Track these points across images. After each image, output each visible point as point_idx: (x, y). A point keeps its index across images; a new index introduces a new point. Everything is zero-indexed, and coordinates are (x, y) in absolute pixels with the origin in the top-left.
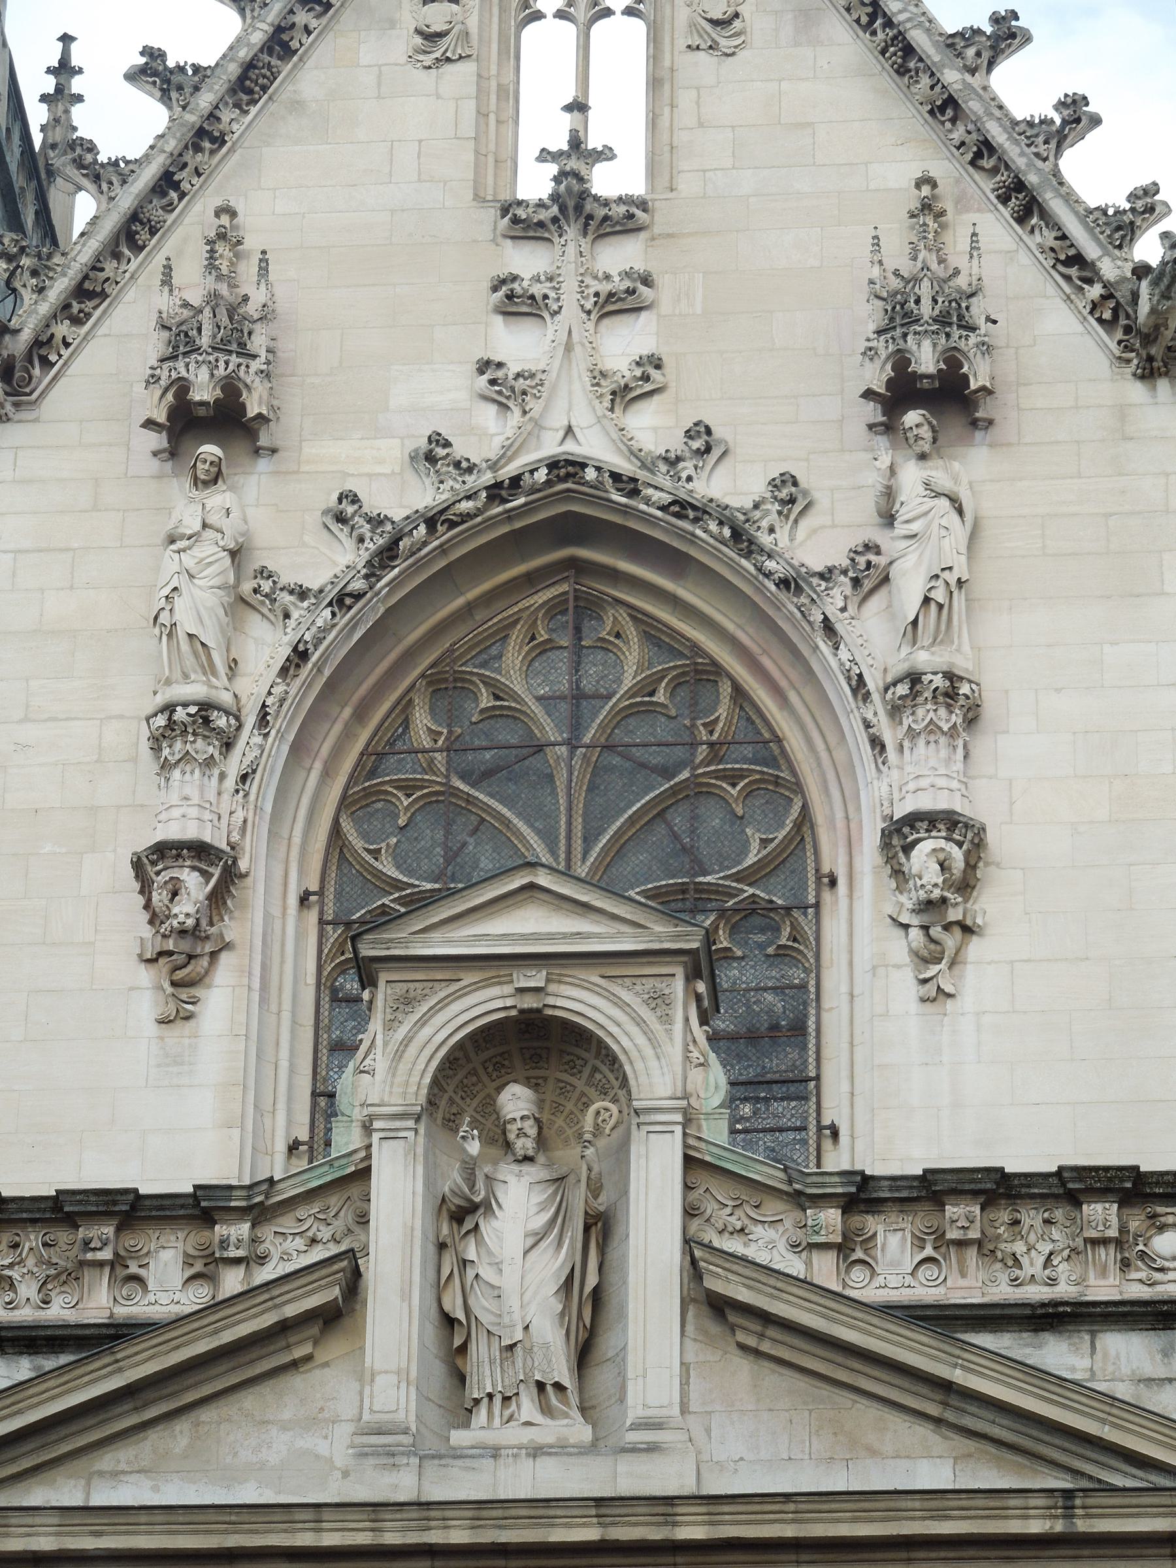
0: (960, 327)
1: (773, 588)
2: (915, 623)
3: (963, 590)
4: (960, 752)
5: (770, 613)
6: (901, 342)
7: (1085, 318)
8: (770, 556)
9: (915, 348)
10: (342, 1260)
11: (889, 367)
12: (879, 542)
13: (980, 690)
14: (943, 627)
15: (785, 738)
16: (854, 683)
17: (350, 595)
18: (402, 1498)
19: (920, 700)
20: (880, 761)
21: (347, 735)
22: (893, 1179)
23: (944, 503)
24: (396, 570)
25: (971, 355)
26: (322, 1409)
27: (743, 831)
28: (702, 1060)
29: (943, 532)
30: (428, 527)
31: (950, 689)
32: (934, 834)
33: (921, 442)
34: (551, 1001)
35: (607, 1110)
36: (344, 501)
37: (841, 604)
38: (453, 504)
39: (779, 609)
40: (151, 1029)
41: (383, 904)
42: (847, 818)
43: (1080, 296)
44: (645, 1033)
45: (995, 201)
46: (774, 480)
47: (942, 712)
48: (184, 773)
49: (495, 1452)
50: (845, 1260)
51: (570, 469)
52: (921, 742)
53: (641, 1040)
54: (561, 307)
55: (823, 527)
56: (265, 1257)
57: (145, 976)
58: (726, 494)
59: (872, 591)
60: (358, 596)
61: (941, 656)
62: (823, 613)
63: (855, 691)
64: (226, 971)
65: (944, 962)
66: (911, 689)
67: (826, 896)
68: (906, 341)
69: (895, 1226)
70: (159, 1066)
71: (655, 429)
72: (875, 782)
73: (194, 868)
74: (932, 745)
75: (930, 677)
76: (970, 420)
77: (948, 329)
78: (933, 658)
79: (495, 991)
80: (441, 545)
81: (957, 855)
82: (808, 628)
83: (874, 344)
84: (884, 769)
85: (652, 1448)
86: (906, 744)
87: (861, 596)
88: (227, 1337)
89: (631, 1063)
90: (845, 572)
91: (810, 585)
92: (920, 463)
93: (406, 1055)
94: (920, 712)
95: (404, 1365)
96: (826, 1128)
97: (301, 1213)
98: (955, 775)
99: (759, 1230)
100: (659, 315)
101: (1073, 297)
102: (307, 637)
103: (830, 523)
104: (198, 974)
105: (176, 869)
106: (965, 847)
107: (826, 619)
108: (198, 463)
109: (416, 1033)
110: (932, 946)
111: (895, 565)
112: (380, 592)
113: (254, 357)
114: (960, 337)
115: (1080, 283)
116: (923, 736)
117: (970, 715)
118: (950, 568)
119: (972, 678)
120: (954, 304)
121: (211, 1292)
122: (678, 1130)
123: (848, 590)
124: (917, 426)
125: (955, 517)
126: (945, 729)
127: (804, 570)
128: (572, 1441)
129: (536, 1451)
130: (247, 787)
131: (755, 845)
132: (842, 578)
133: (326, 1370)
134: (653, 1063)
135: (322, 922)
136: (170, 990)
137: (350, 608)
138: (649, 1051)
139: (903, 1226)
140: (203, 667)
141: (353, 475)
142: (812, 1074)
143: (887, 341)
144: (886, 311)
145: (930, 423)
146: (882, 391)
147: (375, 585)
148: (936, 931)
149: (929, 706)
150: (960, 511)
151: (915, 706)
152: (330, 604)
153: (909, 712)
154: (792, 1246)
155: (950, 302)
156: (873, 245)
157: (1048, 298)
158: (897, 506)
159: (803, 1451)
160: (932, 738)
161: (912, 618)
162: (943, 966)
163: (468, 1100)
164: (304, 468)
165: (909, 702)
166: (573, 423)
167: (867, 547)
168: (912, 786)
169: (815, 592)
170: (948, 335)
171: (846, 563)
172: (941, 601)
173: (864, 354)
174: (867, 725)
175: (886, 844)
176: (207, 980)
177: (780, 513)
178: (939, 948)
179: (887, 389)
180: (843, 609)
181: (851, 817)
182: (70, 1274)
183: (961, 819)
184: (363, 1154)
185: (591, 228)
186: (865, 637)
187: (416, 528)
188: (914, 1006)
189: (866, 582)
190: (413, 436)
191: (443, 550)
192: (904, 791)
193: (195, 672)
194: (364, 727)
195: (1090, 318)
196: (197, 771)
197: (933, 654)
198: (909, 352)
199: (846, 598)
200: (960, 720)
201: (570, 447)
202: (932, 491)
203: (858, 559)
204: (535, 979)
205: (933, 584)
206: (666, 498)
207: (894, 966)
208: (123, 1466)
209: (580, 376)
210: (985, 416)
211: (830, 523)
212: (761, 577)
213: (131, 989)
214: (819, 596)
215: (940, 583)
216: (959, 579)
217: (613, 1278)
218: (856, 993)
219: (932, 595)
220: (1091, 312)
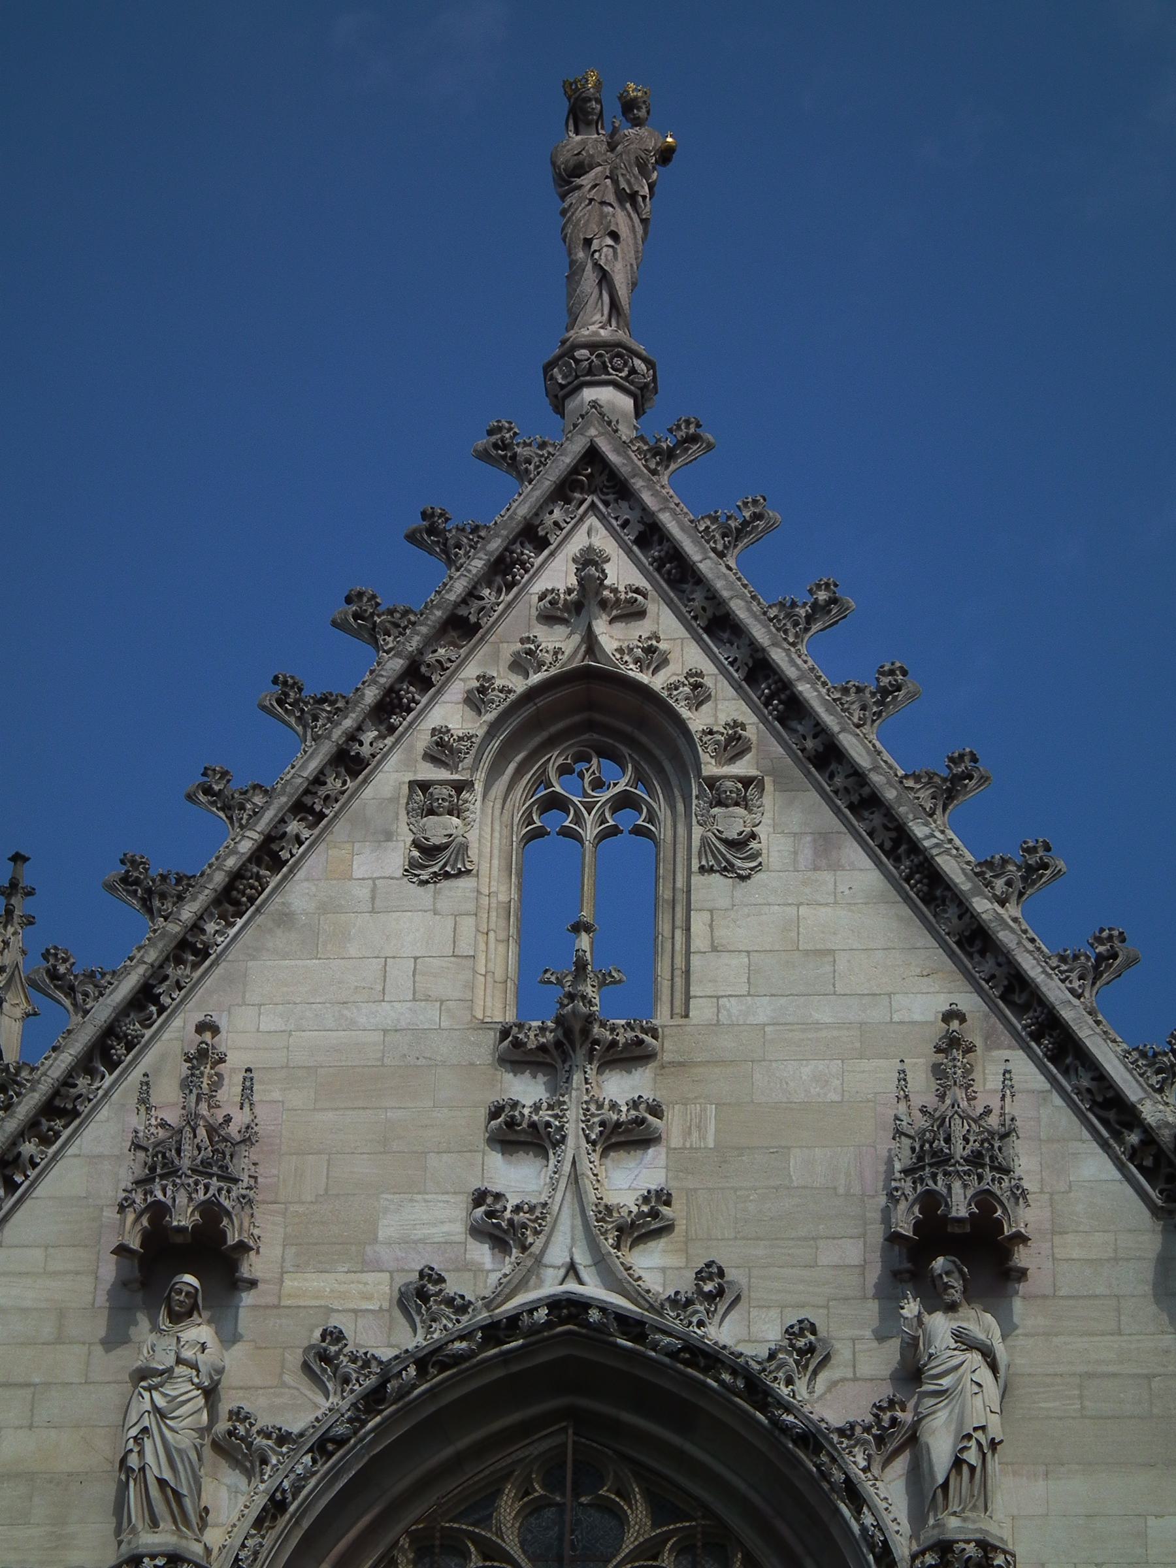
0: (992, 1168)
11: (916, 1209)
46: (792, 1327)
75: (962, 1545)
87: (886, 1455)
114: (993, 1180)
127: (824, 1425)
137: (331, 1454)
141: (338, 1311)
145: (961, 1272)
164: (286, 1302)
170: (980, 1178)
171: (869, 1419)
172: (973, 1462)
190: (403, 1270)
205: (965, 1443)
211: (851, 1375)
212: (777, 1433)
219: (965, 1456)
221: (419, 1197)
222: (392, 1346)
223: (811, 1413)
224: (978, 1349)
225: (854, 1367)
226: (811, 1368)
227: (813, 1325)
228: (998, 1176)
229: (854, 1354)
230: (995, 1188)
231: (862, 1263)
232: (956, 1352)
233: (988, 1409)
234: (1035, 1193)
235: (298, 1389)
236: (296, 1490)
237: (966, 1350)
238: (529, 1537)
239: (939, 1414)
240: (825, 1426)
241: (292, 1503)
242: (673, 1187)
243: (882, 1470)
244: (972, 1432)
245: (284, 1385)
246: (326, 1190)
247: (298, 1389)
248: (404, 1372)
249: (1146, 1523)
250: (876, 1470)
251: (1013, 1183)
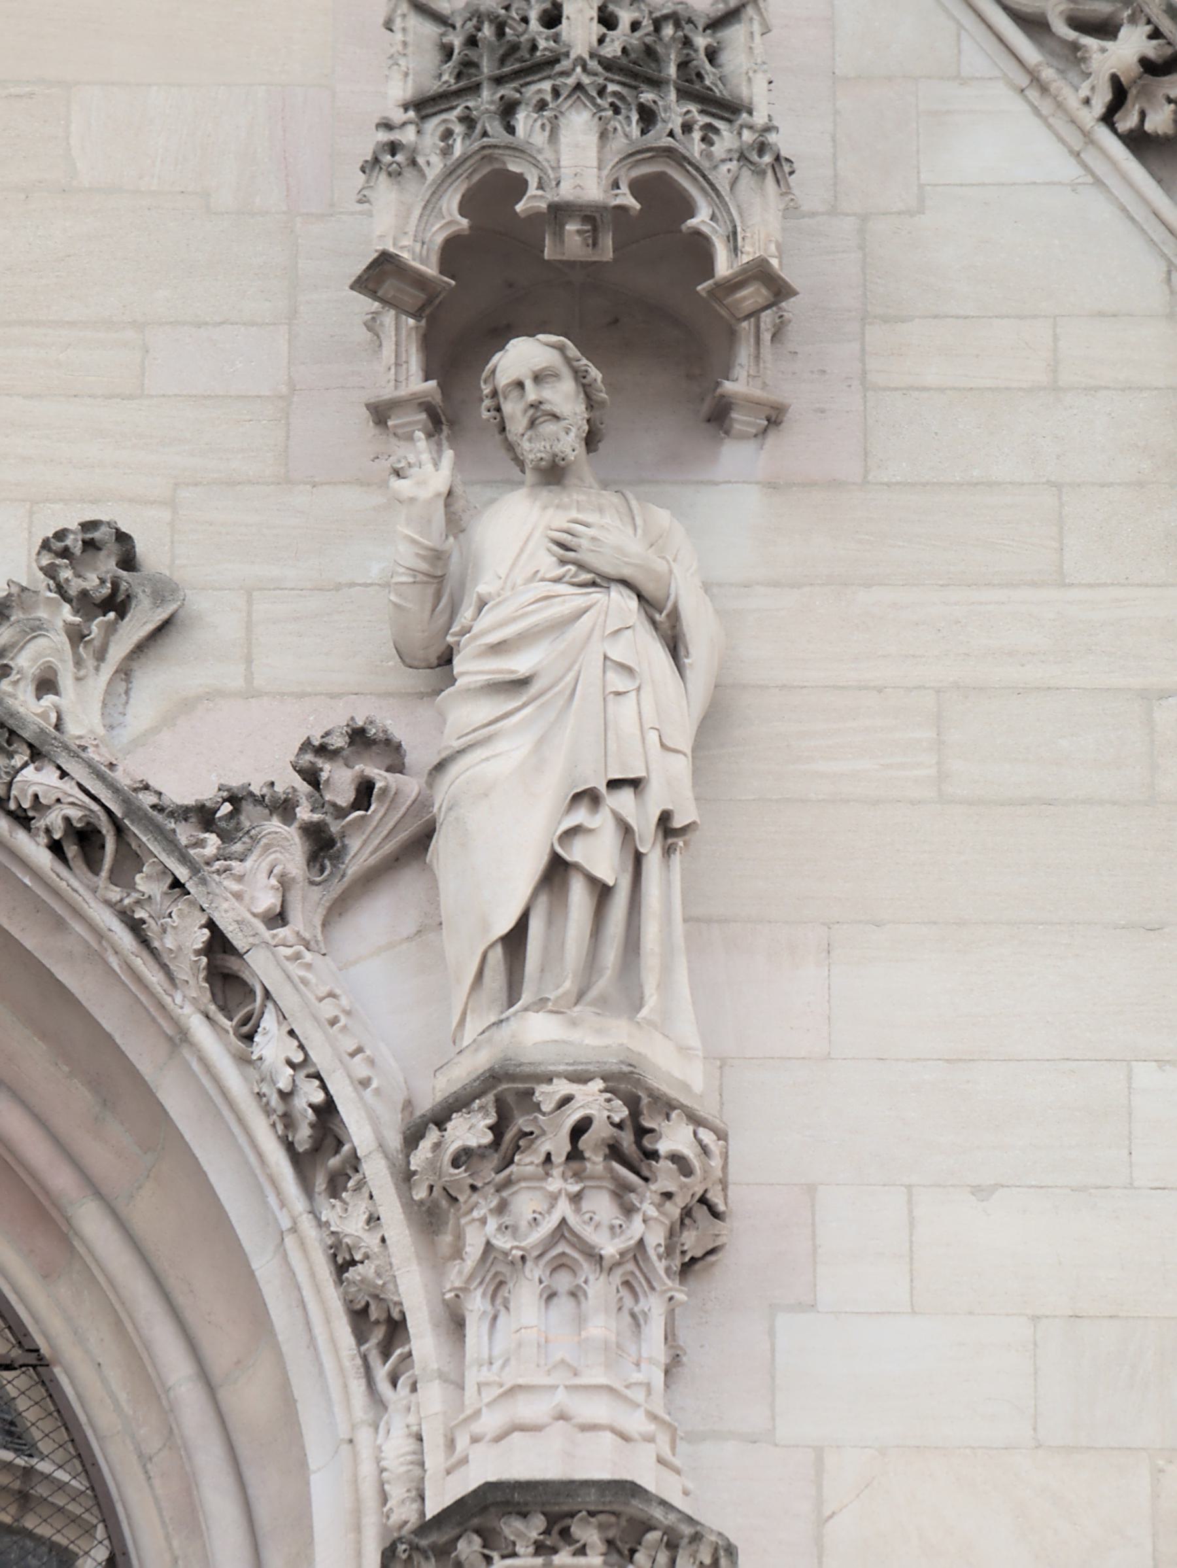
0: (684, 94)
1: (43, 858)
3: (676, 858)
4: (655, 1329)
5: (29, 944)
6: (495, 127)
7: (1087, 136)
8: (36, 754)
9: (539, 139)
11: (451, 202)
12: (398, 733)
13: (725, 1156)
14: (611, 953)
16: (303, 1136)
19: (527, 1163)
20: (381, 1372)
23: (623, 603)
25: (721, 176)
29: (617, 681)
31: (627, 1140)
33: (549, 428)
37: (268, 900)
39: (60, 924)
43: (1073, 75)
46: (61, 535)
47: (602, 1205)
55: (212, 695)
59: (372, 878)
61: (599, 1032)
62: (211, 925)
63: (301, 1162)
66: (497, 1130)
68: (511, 130)
72: (364, 1436)
74: (564, 1304)
75: (562, 1087)
76: (706, 408)
77: (647, 97)
78: (575, 1035)
82: (154, 977)
84: (396, 1398)
86: (476, 1305)
87: (337, 888)
90: (284, 808)
91: (169, 841)
92: (545, 494)
94: (525, 1203)
98: (639, 1395)
101: (1048, 74)
103: (238, 683)
111: (453, 770)
114: (687, 128)
115: (1071, 35)
116: (535, 1271)
117: (691, 1241)
118: (635, 784)
119: (702, 1112)
120: (668, 31)
124: (538, 378)
126: (610, 1249)
127: (147, 799)
132: (275, 824)
143: (448, 134)
144: (447, 52)
145: (579, 375)
146: (431, 270)
149: (555, 1184)
150: (675, 645)
151: (508, 1183)
153: (485, 1204)
155: (657, 24)
157: (964, 81)
158: (466, 614)
160: (563, 1282)
161: (505, 924)
165: (487, 1172)
167: (359, 737)
168: (491, 1422)
169: (184, 859)
170: (648, 117)
171: (289, 781)
173: (373, 164)
177: (77, 636)
179: (444, 267)
180: (278, 918)
183: (658, 1513)
186: (344, 1002)
189: (354, 844)
192: (462, 1442)
195: (1104, 134)
198: (517, 150)
199: (285, 884)
200: (656, 1238)
202: (581, 566)
203: (327, 769)
205: (580, 816)
210: (757, 392)
211: (238, 683)
214: (195, 870)
215: (601, 822)
216: (665, 818)
219: (575, 853)
220: (1108, 118)
223: (112, 766)
224: (625, 583)
225: (249, 660)
227: (122, 538)
228: (703, 120)
229: (249, 627)
230: (695, 147)
231: (284, 390)
232: (561, 588)
233: (653, 737)
234: (813, 214)
237: (594, 584)
239: (501, 746)
240: (153, 799)
243: (325, 924)
244: (603, 789)
249: (1130, 1078)
250: (304, 919)
251: (747, 136)
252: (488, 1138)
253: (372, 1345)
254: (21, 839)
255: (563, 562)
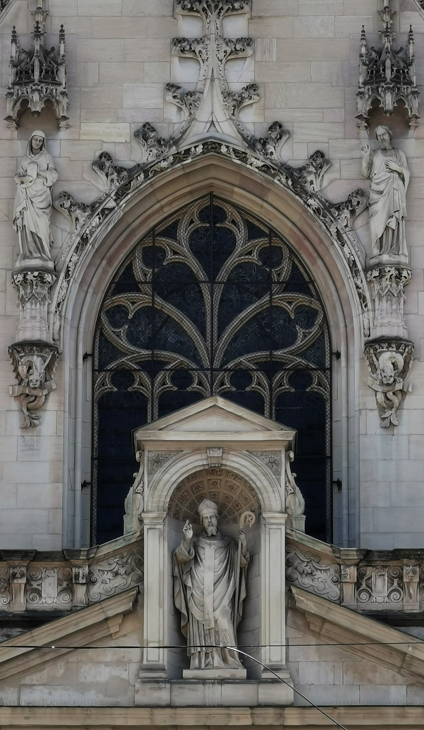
1: (312, 212)
2: (381, 238)
10: (133, 591)
15: (315, 281)
17: (108, 209)
18: (163, 703)
19: (384, 279)
20: (363, 305)
21: (105, 272)
22: (380, 552)
23: (397, 175)
24: (129, 196)
26: (124, 657)
27: (295, 327)
28: (293, 491)
30: (145, 175)
32: (390, 349)
34: (224, 462)
35: (250, 516)
36: (103, 158)
38: (157, 163)
40: (18, 432)
41: (123, 361)
42: (346, 326)
44: (268, 480)
45: (420, 7)
48: (32, 303)
49: (203, 681)
50: (357, 590)
51: (213, 146)
52: (384, 300)
53: (266, 483)
54: (208, 58)
55: (335, 179)
56: (95, 582)
57: (14, 405)
58: (289, 160)
60: (111, 210)
61: (394, 258)
64: (52, 404)
65: (393, 409)
66: (380, 273)
67: (335, 363)
69: (380, 573)
70: (23, 450)
71: (254, 123)
73: (38, 356)
74: (389, 302)
77: (398, 86)
79: (198, 457)
80: (151, 182)
81: (400, 360)
83: (362, 90)
84: (366, 310)
85: (274, 681)
88: (82, 626)
89: (261, 494)
91: (330, 212)
93: (158, 487)
95: (161, 639)
96: (335, 482)
97: (111, 561)
99: (318, 574)
100: (255, 61)
102: (88, 232)
103: (339, 177)
104: (40, 405)
105: (30, 357)
106: (404, 355)
107: (338, 231)
108: (33, 141)
109: (163, 477)
110: (388, 402)
112: (121, 206)
113: (60, 84)
116: (385, 297)
121: (71, 598)
122: (283, 527)
123: (348, 216)
125: (401, 182)
128: (237, 676)
129: (222, 681)
130: (60, 309)
131: (300, 336)
133: (125, 638)
134: (272, 495)
135: (93, 370)
136: (27, 413)
137: (107, 215)
138: (270, 489)
139: (384, 573)
140: (38, 248)
141: (106, 142)
142: (329, 455)
145: (389, 133)
147: (119, 203)
148: (390, 395)
152: (98, 214)
154: (334, 582)
156: (362, 35)
159: (340, 681)
160: (389, 297)
161: (380, 236)
162: (393, 411)
163: (184, 503)
164: (82, 138)
166: (214, 120)
172: (394, 228)
174: (358, 287)
175: (366, 351)
176: (44, 407)
178: (391, 403)
181: (347, 325)
182: (6, 588)
184: (138, 534)
185: (221, 14)
187: (139, 175)
188: (379, 431)
189: (357, 211)
190: (135, 122)
191: (151, 184)
193: (36, 252)
194: (111, 267)
196: (38, 304)
197: (390, 256)
201: (212, 133)
204: (217, 453)
206: (260, 164)
207: (369, 410)
208: (34, 682)
209: (217, 95)
211: (339, 177)
212: (306, 206)
213: (7, 411)
217: (253, 593)
218: (349, 416)
221: (141, 85)
222: (132, 161)
226: (321, 175)
235: (90, 181)
236: (92, 233)
238: (194, 242)
241: (90, 239)
242: (258, 80)
245: (84, 179)
246: (99, 81)
247: (90, 181)
248: (139, 177)
252: (378, 275)
253: (361, 300)
254: (309, 209)
255: (387, 168)
